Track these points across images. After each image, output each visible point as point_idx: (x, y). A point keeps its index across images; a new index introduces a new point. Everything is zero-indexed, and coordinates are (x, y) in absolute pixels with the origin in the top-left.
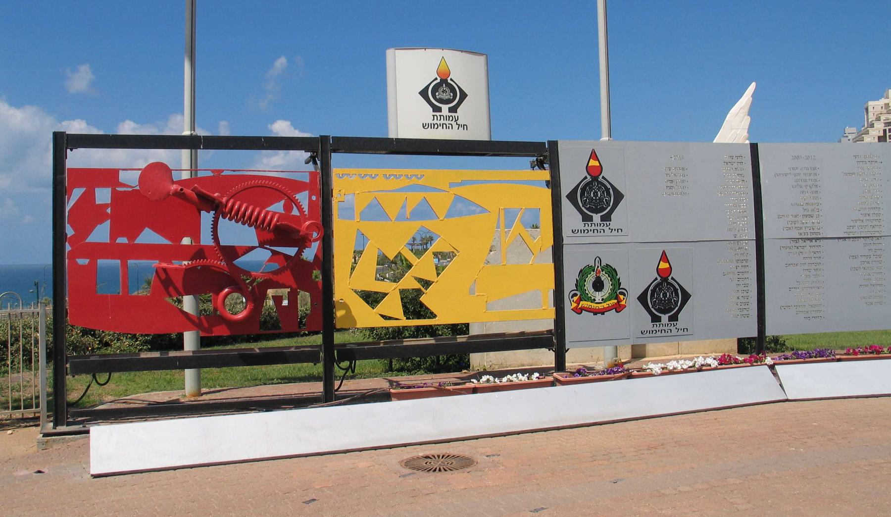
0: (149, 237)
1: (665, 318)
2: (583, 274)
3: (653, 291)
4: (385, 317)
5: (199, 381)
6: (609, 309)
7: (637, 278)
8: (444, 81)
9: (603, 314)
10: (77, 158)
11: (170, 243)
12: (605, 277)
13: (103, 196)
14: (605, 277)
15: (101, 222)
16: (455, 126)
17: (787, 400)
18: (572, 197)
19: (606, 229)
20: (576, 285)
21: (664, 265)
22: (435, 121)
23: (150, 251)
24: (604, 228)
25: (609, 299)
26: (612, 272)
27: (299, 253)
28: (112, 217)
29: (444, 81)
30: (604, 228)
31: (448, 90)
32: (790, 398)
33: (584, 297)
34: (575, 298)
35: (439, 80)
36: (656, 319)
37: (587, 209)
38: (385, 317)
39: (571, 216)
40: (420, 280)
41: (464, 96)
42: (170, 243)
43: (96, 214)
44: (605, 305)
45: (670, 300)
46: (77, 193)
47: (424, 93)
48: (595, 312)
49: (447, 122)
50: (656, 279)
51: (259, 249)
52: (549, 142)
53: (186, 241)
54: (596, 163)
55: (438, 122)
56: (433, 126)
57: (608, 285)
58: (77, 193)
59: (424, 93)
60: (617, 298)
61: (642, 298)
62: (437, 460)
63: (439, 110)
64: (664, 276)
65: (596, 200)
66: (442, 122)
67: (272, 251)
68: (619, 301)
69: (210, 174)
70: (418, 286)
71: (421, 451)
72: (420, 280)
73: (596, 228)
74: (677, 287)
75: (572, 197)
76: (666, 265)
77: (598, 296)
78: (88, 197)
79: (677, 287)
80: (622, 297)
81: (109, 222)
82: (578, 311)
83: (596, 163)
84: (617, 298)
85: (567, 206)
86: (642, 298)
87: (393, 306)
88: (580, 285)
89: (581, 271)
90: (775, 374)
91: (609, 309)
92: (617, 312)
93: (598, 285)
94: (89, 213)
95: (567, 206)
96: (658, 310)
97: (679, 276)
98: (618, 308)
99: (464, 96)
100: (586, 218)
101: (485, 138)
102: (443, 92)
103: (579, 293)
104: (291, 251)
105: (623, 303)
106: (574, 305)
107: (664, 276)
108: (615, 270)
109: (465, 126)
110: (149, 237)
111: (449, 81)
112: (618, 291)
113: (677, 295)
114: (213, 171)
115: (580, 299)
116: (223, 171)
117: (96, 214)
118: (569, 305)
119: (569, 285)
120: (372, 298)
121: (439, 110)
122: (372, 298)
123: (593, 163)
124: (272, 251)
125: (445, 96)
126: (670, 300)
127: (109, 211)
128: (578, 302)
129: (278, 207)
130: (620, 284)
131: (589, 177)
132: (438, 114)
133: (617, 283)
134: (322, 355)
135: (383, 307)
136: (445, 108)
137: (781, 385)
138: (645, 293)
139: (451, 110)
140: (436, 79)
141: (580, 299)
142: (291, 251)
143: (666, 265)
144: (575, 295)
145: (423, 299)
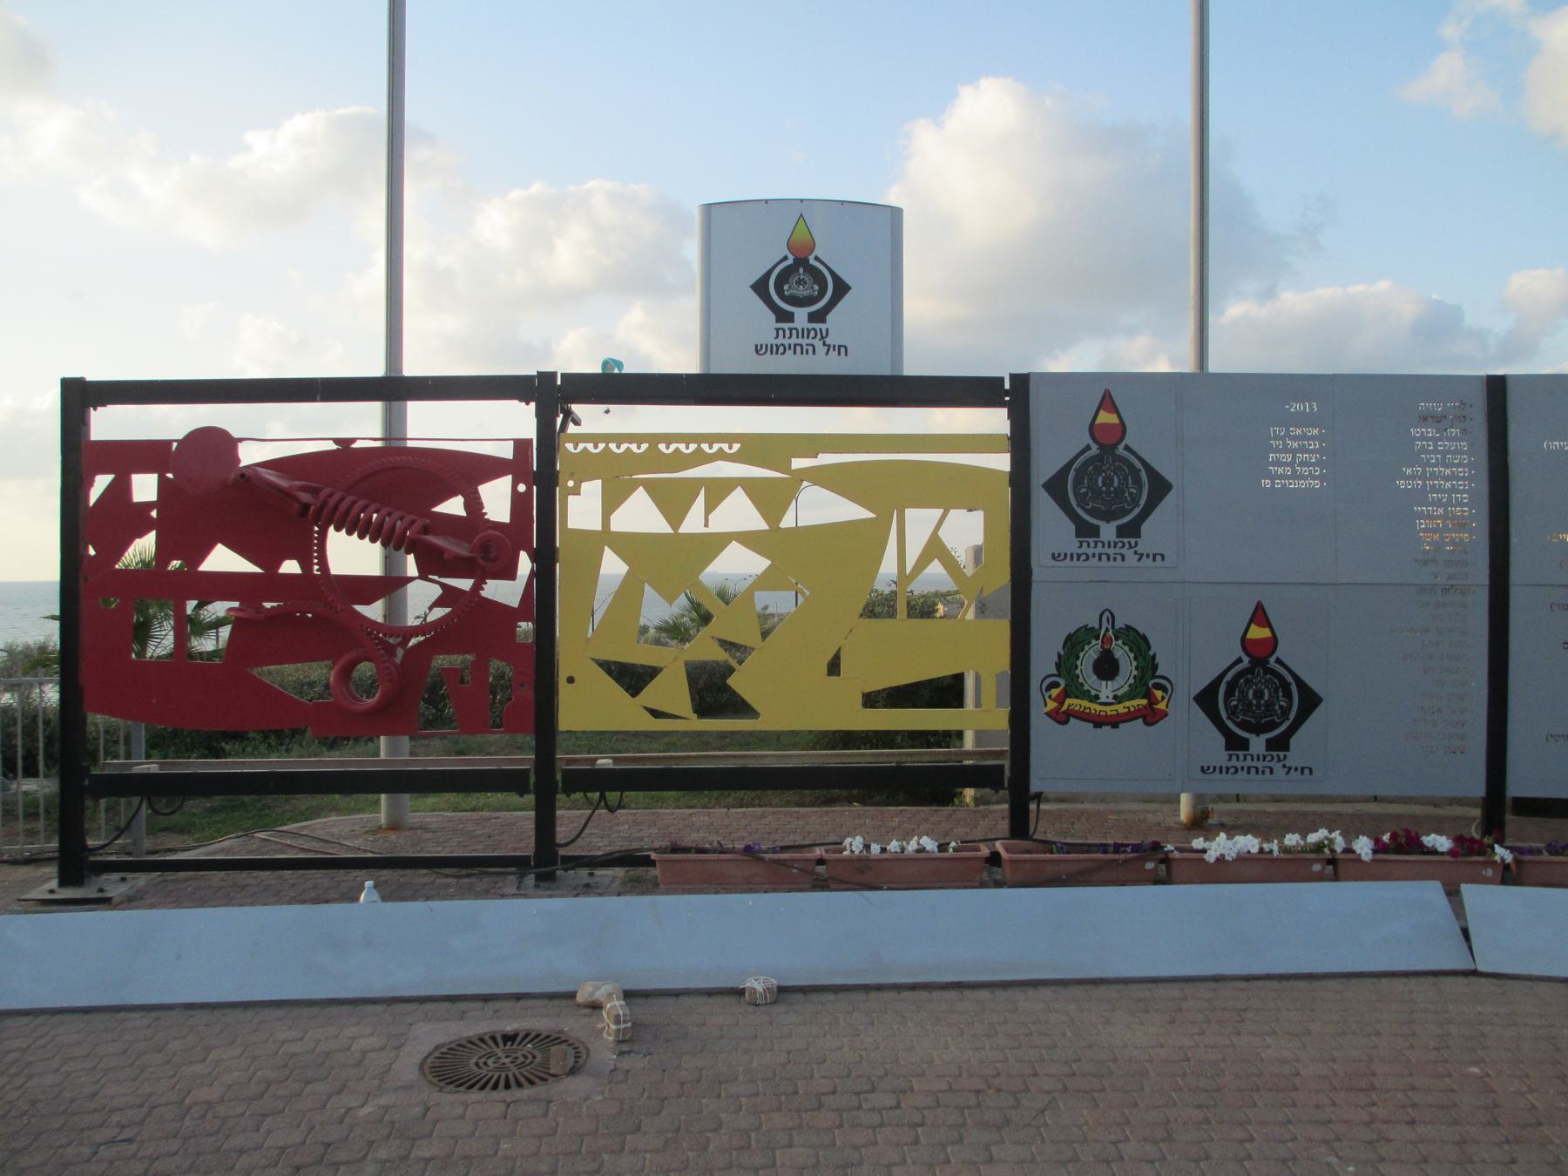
0: (222, 560)
1: (1257, 743)
2: (1074, 643)
3: (1232, 685)
4: (656, 714)
5: (393, 807)
6: (1129, 717)
7: (1197, 654)
8: (801, 262)
9: (1115, 725)
10: (108, 424)
11: (258, 570)
12: (1121, 652)
13: (145, 487)
14: (1121, 652)
15: (141, 534)
16: (821, 349)
17: (1475, 973)
18: (1055, 486)
19: (1128, 553)
20: (1058, 666)
21: (1257, 633)
22: (780, 340)
23: (224, 584)
24: (1124, 551)
25: (1130, 696)
26: (1138, 642)
27: (477, 587)
28: (161, 527)
29: (801, 262)
30: (1124, 551)
31: (807, 278)
32: (1481, 968)
33: (1074, 689)
34: (1055, 692)
35: (790, 261)
36: (1235, 744)
37: (1087, 512)
38: (656, 714)
39: (1052, 527)
40: (727, 645)
41: (842, 288)
42: (258, 570)
43: (134, 520)
44: (1120, 708)
45: (1269, 705)
46: (102, 482)
47: (760, 287)
48: (1098, 722)
49: (804, 342)
50: (1239, 660)
51: (418, 581)
52: (1013, 377)
53: (290, 567)
54: (1112, 419)
55: (786, 342)
56: (775, 349)
57: (1128, 668)
58: (102, 482)
59: (760, 287)
60: (1147, 694)
61: (1206, 699)
62: (506, 1053)
63: (789, 317)
64: (1259, 656)
65: (1108, 494)
66: (794, 340)
67: (443, 585)
68: (1153, 701)
69: (332, 446)
70: (720, 655)
71: (481, 1024)
72: (724, 644)
73: (1106, 550)
74: (1289, 679)
75: (1055, 486)
76: (1265, 633)
77: (1106, 690)
78: (121, 489)
79: (1289, 679)
80: (1159, 694)
81: (765, 526)
82: (1060, 717)
83: (1112, 419)
84: (1147, 694)
85: (1044, 507)
86: (1206, 699)
87: (671, 692)
88: (1065, 664)
89: (1069, 638)
90: (1459, 909)
91: (1129, 717)
92: (1147, 723)
93: (1106, 667)
94: (122, 518)
95: (1044, 507)
96: (1241, 725)
97: (1294, 655)
98: (1151, 716)
99: (842, 288)
100: (1085, 531)
101: (888, 373)
102: (799, 282)
103: (1062, 682)
104: (465, 584)
105: (1162, 706)
106: (1052, 705)
107: (1259, 656)
108: (1144, 638)
109: (842, 349)
110: (222, 560)
111: (812, 261)
112: (1149, 678)
113: (1288, 695)
114: (336, 441)
115: (1065, 694)
116: (354, 440)
117: (134, 520)
118: (1040, 707)
119: (1043, 663)
120: (633, 678)
121: (789, 317)
122: (633, 678)
123: (1105, 418)
124: (443, 585)
125: (802, 291)
126: (1269, 705)
127: (154, 514)
128: (1060, 700)
129: (454, 506)
130: (1155, 667)
131: (1094, 447)
132: (786, 326)
133: (1148, 664)
134: (532, 779)
135: (652, 694)
136: (801, 315)
137: (1465, 933)
138: (1214, 686)
139: (813, 318)
140: (786, 258)
141: (1065, 694)
142: (465, 584)
143: (1265, 633)
144: (1055, 685)
145: (730, 681)
